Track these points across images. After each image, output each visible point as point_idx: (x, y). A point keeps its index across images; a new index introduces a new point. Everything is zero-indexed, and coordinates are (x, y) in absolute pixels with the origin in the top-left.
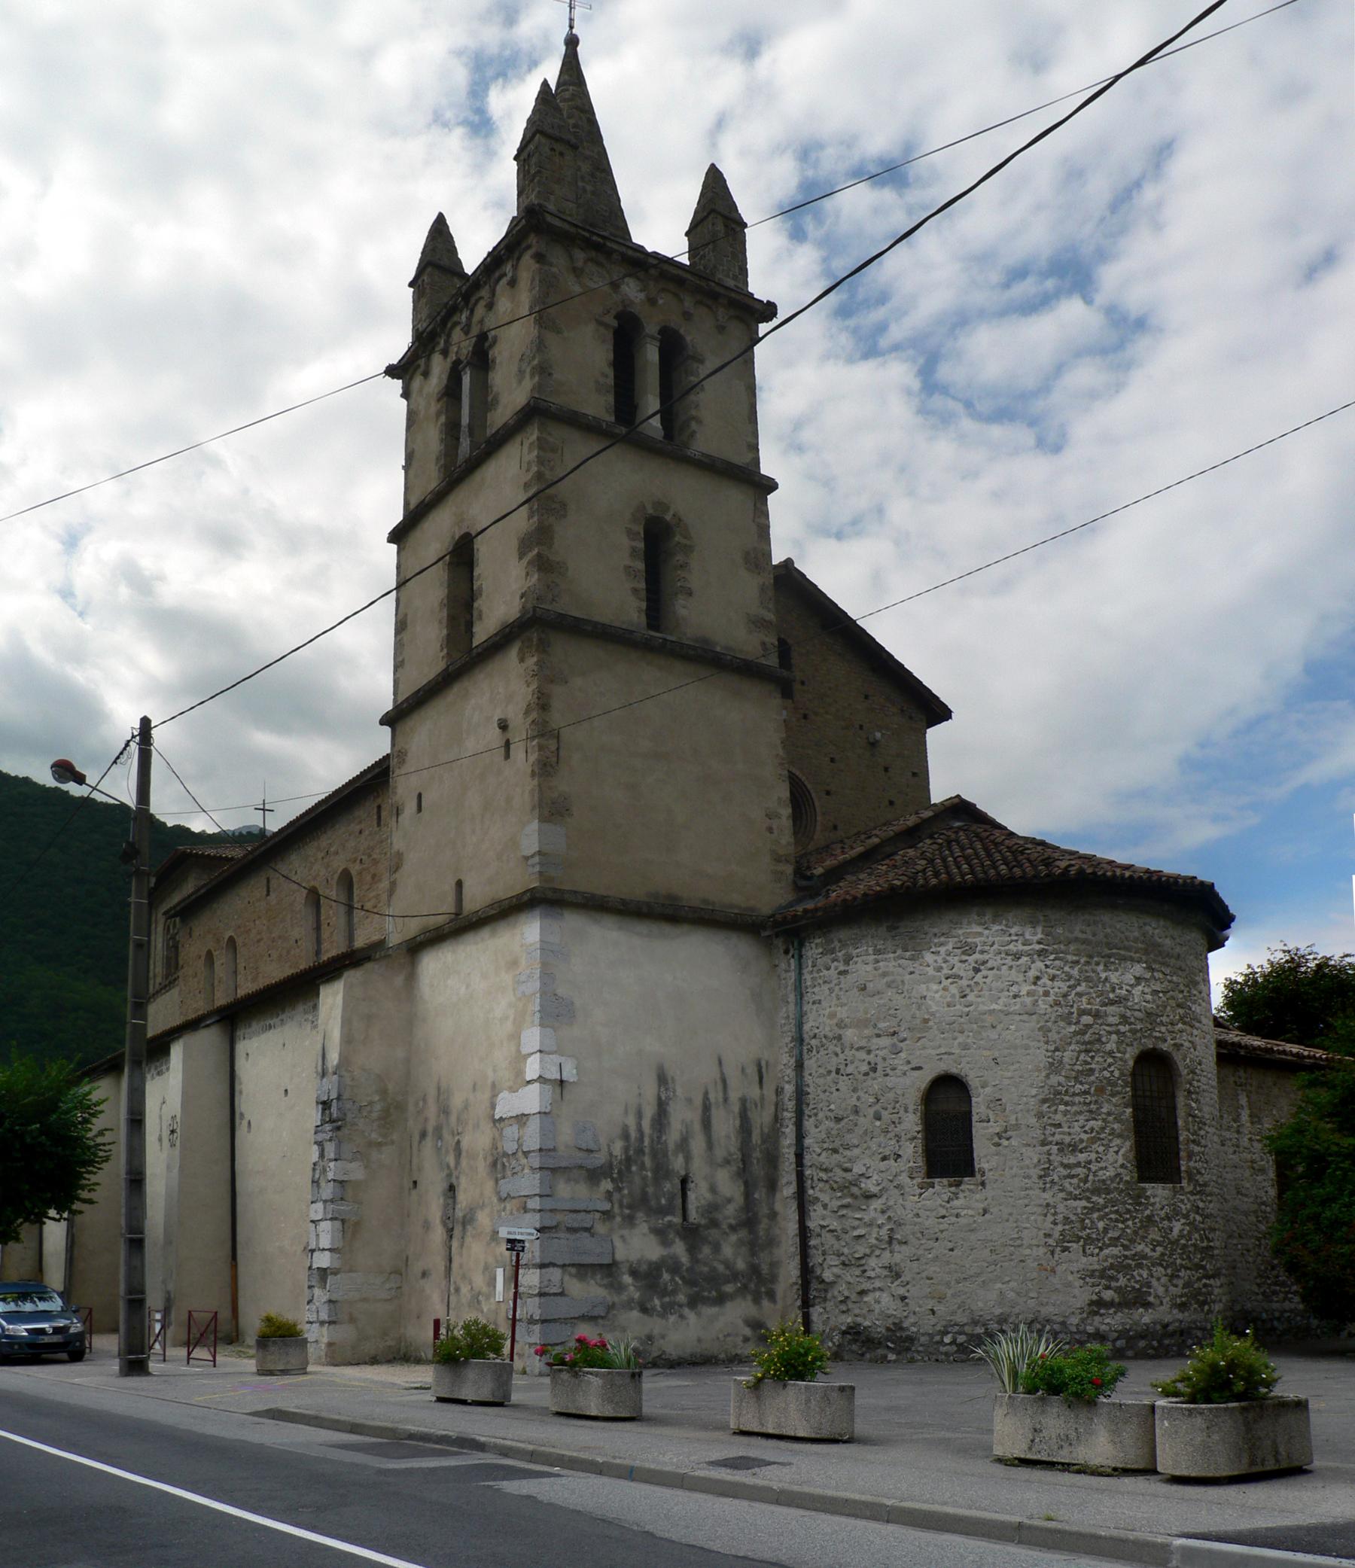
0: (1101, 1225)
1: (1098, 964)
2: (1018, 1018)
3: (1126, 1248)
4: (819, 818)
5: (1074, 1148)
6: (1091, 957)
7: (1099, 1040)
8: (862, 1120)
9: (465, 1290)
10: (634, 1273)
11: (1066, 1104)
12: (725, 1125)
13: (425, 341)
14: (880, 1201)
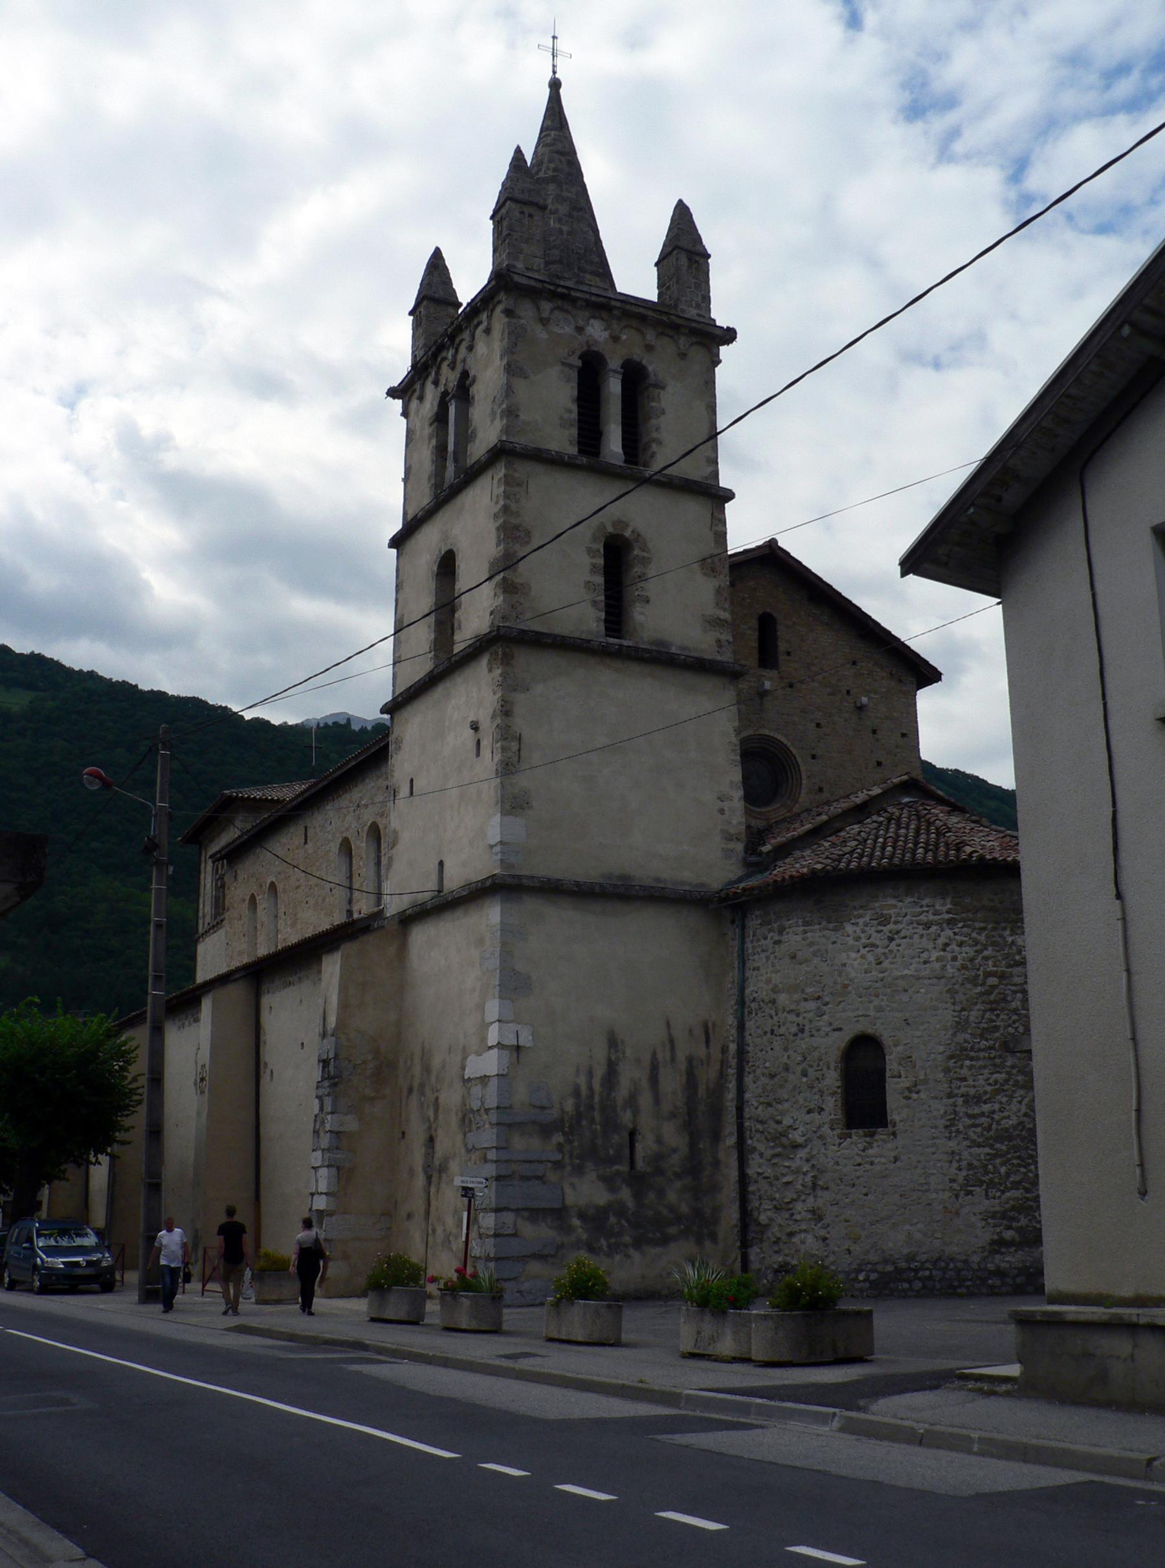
0: (1003, 1170)
1: (1004, 929)
2: (927, 982)
3: (1027, 1190)
4: (804, 782)
5: (978, 1099)
6: (998, 923)
7: (1004, 1000)
8: (791, 1077)
9: (439, 1230)
10: (582, 1216)
11: (972, 1059)
12: (672, 1083)
13: (421, 370)
14: (807, 1150)
